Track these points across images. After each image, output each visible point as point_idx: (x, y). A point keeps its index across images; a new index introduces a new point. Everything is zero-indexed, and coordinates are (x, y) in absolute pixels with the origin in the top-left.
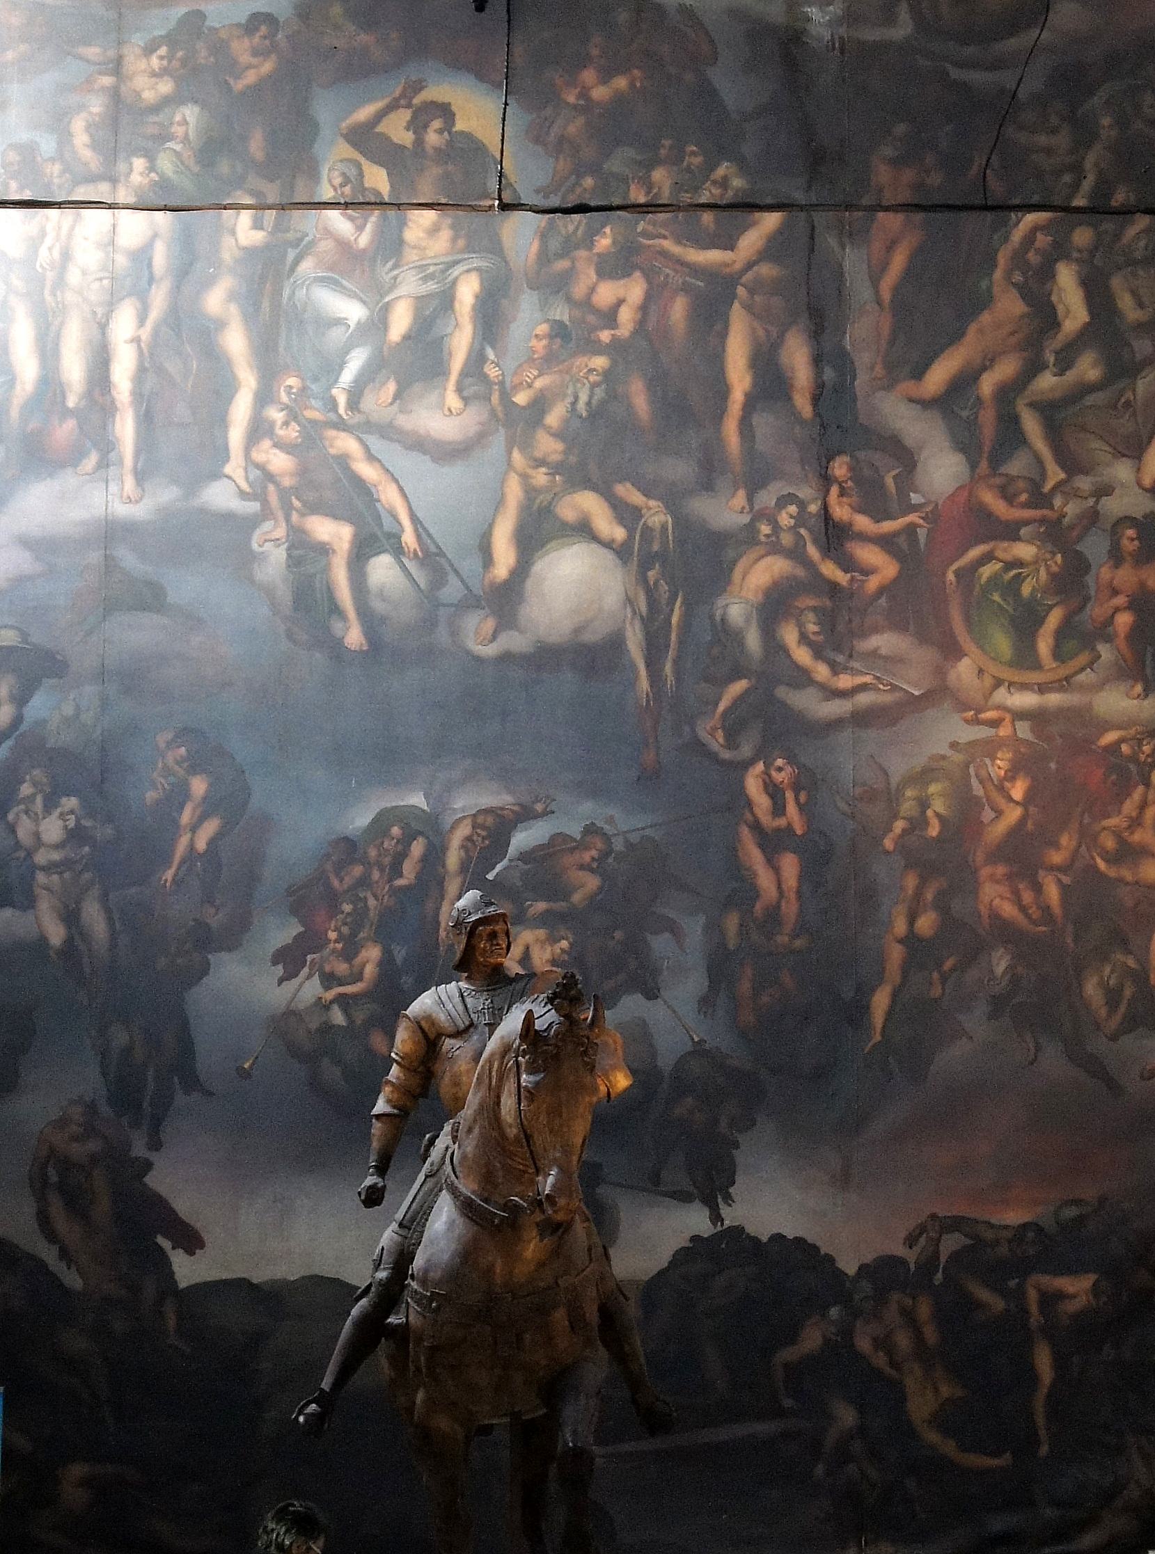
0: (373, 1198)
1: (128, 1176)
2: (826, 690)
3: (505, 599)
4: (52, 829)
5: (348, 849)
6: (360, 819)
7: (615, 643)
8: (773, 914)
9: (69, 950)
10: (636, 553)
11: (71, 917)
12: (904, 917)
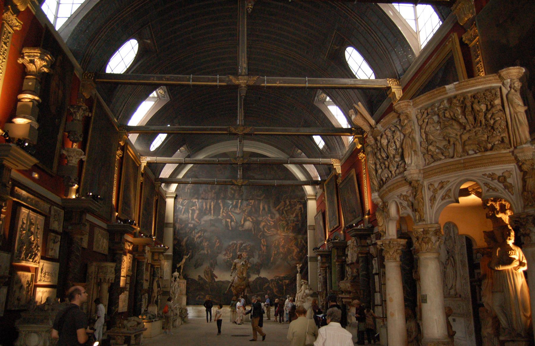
0: (231, 276)
1: (212, 272)
2: (268, 233)
3: (243, 226)
4: (206, 244)
5: (230, 246)
6: (231, 243)
7: (251, 229)
8: (264, 252)
9: (207, 254)
10: (253, 222)
11: (207, 251)
12: (273, 252)
